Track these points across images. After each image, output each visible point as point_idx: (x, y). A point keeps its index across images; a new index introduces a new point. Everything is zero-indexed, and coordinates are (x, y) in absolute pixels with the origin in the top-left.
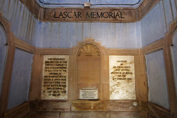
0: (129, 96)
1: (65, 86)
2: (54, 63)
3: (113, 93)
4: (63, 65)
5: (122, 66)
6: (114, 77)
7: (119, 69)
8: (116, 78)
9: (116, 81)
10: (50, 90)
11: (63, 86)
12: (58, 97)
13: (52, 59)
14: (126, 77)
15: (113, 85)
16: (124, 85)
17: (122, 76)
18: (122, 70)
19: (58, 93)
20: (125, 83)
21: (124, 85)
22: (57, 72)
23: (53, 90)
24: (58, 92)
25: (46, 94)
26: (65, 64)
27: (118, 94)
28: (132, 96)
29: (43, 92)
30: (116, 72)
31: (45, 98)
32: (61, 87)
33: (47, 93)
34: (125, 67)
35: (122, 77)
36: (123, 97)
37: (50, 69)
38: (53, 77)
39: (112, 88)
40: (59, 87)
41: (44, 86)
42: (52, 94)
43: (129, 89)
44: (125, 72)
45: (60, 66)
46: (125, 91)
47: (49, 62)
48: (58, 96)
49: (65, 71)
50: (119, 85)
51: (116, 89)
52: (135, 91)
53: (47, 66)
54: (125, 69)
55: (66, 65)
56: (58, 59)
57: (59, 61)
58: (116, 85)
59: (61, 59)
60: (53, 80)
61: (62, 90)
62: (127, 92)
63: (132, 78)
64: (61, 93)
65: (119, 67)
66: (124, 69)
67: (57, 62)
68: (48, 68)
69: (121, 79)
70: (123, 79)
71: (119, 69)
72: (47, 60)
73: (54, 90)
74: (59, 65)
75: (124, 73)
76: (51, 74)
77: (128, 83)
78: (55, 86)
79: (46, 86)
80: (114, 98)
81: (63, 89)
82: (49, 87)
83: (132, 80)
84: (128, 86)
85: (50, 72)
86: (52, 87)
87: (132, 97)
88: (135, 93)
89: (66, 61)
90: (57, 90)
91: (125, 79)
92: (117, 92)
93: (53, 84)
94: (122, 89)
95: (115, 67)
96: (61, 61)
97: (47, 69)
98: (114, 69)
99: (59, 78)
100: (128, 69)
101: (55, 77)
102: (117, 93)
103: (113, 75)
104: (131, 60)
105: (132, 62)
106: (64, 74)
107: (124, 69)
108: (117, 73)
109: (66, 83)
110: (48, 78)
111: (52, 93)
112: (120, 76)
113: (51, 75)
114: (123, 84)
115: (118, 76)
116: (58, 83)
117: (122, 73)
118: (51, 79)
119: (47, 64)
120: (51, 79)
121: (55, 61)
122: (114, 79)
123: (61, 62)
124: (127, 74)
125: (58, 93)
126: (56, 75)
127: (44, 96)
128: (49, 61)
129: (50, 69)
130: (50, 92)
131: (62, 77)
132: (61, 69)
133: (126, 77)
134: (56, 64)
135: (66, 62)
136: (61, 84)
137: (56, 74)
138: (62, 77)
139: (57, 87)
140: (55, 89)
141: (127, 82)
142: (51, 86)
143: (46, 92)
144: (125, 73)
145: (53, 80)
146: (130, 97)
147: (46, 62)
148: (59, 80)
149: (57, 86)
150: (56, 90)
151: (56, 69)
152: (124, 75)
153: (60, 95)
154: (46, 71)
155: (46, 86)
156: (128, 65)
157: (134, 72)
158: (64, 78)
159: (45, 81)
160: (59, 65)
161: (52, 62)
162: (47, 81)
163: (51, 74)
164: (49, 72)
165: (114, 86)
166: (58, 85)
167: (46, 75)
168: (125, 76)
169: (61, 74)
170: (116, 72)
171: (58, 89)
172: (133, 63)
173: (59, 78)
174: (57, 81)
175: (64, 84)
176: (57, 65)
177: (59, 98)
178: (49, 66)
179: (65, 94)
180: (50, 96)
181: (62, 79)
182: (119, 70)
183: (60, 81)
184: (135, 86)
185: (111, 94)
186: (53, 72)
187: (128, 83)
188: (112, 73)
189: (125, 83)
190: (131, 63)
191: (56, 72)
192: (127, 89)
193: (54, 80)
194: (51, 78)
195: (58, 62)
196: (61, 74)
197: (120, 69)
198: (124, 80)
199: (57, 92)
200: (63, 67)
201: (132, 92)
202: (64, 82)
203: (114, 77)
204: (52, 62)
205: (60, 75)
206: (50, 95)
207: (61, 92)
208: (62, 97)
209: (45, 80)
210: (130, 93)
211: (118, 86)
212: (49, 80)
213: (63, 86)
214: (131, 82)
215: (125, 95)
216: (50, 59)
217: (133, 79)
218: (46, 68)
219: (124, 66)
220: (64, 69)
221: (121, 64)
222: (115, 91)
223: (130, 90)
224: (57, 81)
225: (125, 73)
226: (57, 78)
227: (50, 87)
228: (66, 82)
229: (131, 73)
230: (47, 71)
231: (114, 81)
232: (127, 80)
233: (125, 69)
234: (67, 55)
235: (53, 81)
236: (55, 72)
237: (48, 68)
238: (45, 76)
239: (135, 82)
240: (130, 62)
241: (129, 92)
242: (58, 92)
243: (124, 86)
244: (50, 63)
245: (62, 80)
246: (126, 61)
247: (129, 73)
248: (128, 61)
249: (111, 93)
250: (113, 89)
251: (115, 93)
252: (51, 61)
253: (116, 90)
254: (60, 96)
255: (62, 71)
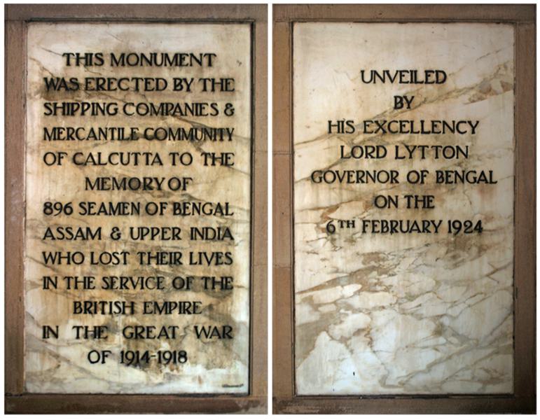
0: (459, 364)
1: (226, 285)
2: (118, 96)
3: (323, 338)
4: (198, 109)
5: (406, 115)
6: (332, 209)
7: (374, 139)
8: (351, 224)
9: (352, 241)
10: (99, 319)
11: (209, 284)
12: (170, 378)
13: (100, 57)
14: (437, 214)
15: (329, 278)
16: (415, 278)
17: (402, 202)
18: (402, 152)
19: (165, 346)
20: (430, 258)
21: (422, 280)
22: (154, 171)
23: (120, 320)
24: (168, 332)
25: (64, 352)
26: (220, 100)
27: (366, 355)
28: (487, 363)
29: (40, 333)
30: (351, 165)
31: (55, 381)
32: (190, 296)
33: (69, 344)
34: (434, 125)
35: (400, 214)
36: (411, 376)
37: (88, 148)
38: (120, 209)
39: (316, 307)
40: (177, 297)
41: (48, 282)
42: (117, 351)
43: (456, 310)
44: (431, 165)
45: (172, 122)
46: (424, 332)
47: (74, 81)
48: (166, 370)
49: (225, 160)
50: (373, 277)
51: (349, 307)
52: (510, 322)
53: (63, 122)
54: (429, 140)
55: (230, 110)
56: (152, 60)
57: (168, 74)
58: (353, 276)
59: (179, 59)
60: (116, 234)
61: (202, 320)
62: (439, 332)
63: (489, 218)
64: (189, 345)
65: (383, 127)
66: (420, 140)
67: (147, 81)
68: (72, 134)
69: (392, 228)
70: (413, 228)
71: (374, 139)
72: (57, 67)
73: (132, 320)
74: (166, 110)
75: (422, 175)
76: (101, 184)
77: (456, 262)
78: (143, 283)
79: (62, 284)
80: (334, 380)
81: (210, 307)
82: (87, 295)
83: (487, 240)
84: (456, 283)
85: (93, 172)
86: (112, 297)
87: (482, 374)
88: (510, 342)
89: (224, 73)
90: (157, 321)
91: (426, 227)
92: (358, 332)
93: (117, 272)
94: (403, 312)
95: (340, 127)
96: (181, 73)
97: (61, 146)
98: (336, 142)
99: (175, 221)
100: (461, 140)
101: (136, 209)
102: (359, 344)
103: (326, 195)
104: (487, 67)
105: (496, 85)
106: (213, 183)
107: (420, 140)
108: (361, 176)
109: (231, 261)
110: (75, 222)
111: (117, 342)
112: (390, 202)
113: (98, 197)
114: (412, 270)
115: (367, 207)
116: (160, 262)
117: (402, 178)
118: (106, 232)
119: (60, 99)
120: (106, 232)
121: (125, 72)
122: (330, 230)
123: (179, 84)
124: (443, 188)
125: (165, 346)
126: (144, 198)
127: (48, 365)
128: (81, 73)
129: (88, 148)
130: (98, 332)
131: (198, 208)
132: (186, 146)
133: (437, 214)
134: (136, 99)
135: (226, 85)
136: (187, 270)
137: (147, 187)
138: (198, 208)
139: (160, 296)
140: (139, 307)
141: (443, 250)
142: (109, 284)
143: (67, 332)
144: (430, 179)
145: (116, 234)
146: (468, 375)
147: (52, 85)
148: (176, 236)
149: (159, 285)
150: (147, 321)
151: (141, 145)
152: (419, 191)
153: (183, 355)
154: (58, 158)
155: (62, 284)
156: (457, 111)
157: (511, 171)
158: (214, 222)
159: (51, 247)
160: (166, 110)
161: (102, 85)
162: (69, 247)
163: (101, 184)
164: (81, 174)
165: (334, 283)
166: (168, 281)
167: (57, 194)
168: (427, 202)
169: (183, 183)
170: (351, 165)
171: (168, 307)
172: (505, 87)
173: (175, 221)
174: (157, 241)
175: (215, 272)
176: (152, 111)
177: (179, 378)
178: (75, 122)
179: (227, 348)
180: (97, 369)
181: (200, 226)
182: (377, 152)
183: (184, 245)
184: (509, 282)
185: (307, 353)
186: (117, 171)
187: (456, 262)
188: (317, 177)
189: (430, 258)
190: (485, 90)
191: (141, 172)
192: (440, 310)
193: (125, 235)
194: (106, 224)
195: (160, 85)
196: (183, 183)
197: (392, 142)
198: (417, 240)
199: (156, 332)
200: (205, 130)
201: (485, 331)
202: (217, 255)
203: (335, 215)
204: (99, 87)
205: (177, 197)
206: (103, 356)
207: (191, 337)
208: (200, 370)
209: (48, 234)
210: (464, 339)
211: (368, 288)
212: (86, 235)
213: (209, 284)
214: (482, 250)
215: (428, 357)
216: (88, 57)
217: (493, 231)
218: (52, 134)
219: (425, 113)
220: (209, 147)
221: (400, 102)
222: (337, 330)
223: (466, 321)
224: (147, 243)
225: (430, 179)
226: (157, 222)
227: (97, 294)
228: (228, 255)
229: (486, 180)
230: (66, 161)
231: (335, 248)
232: (443, 234)
233: (429, 140)
234: (236, 27)
235: (119, 248)
236: (131, 172)
237: (72, 134)
238: (48, 208)
239: (509, 255)
240: (475, 80)
241: (455, 334)
242: (168, 332)
243: (415, 290)
244: (82, 97)
245: (194, 233)
246: (439, 77)
247: (463, 178)
248: (464, 77)
249: (311, 344)
250: (325, 309)
251: (344, 340)
252: (94, 71)
253: (353, 321)
254: (186, 368)
255: (197, 156)
